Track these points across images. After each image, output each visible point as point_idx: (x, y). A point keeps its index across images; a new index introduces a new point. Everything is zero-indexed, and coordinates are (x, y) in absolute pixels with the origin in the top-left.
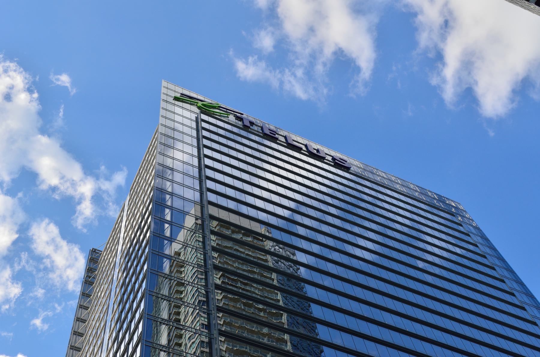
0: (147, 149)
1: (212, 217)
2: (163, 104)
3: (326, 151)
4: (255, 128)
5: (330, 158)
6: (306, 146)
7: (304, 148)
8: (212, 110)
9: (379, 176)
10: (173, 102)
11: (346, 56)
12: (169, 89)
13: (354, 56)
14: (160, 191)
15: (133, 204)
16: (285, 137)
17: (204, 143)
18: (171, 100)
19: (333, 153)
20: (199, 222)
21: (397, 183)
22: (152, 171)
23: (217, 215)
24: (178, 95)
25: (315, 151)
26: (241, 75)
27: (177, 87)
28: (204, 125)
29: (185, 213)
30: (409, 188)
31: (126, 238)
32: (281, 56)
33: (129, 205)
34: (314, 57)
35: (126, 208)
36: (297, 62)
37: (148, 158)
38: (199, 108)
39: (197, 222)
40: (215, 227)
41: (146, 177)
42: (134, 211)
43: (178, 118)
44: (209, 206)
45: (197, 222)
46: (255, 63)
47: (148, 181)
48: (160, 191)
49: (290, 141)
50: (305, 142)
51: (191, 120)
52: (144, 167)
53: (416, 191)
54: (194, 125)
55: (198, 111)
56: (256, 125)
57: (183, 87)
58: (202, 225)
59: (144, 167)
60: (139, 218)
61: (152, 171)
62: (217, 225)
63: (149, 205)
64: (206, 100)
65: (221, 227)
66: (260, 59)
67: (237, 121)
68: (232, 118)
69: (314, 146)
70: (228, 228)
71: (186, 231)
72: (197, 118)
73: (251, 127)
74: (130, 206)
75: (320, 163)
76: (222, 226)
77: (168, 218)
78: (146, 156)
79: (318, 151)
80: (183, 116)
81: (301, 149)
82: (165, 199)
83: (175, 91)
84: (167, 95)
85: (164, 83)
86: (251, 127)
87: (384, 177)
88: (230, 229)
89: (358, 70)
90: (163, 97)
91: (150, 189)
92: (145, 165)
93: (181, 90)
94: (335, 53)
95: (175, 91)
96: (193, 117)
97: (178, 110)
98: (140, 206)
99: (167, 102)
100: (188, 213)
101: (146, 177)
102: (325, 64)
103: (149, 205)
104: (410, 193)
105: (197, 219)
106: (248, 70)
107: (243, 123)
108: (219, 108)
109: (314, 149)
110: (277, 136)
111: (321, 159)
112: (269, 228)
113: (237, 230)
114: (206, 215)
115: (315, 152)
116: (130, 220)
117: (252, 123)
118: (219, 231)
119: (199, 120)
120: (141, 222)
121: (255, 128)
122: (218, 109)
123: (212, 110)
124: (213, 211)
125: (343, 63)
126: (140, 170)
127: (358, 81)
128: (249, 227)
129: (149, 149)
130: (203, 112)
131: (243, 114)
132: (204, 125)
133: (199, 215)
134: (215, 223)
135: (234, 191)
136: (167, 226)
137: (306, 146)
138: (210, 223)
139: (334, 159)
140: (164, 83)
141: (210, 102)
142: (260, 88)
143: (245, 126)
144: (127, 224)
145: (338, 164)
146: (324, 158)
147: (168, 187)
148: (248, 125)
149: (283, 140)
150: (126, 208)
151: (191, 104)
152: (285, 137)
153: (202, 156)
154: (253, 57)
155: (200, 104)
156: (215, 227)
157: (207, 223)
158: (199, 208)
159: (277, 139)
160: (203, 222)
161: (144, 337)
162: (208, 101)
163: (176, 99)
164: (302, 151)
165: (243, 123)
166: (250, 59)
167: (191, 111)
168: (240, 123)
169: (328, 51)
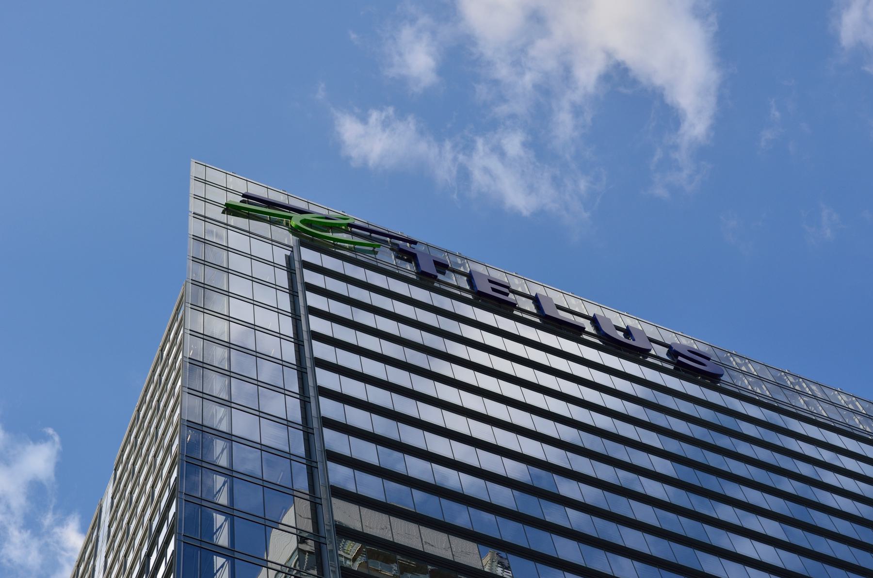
0: (158, 352)
1: (344, 533)
2: (196, 188)
3: (651, 331)
4: (453, 279)
5: (662, 352)
6: (594, 320)
7: (589, 328)
8: (330, 235)
9: (802, 393)
10: (224, 218)
11: (635, 82)
12: (21, 549)
13: (658, 81)
14: (199, 433)
15: (124, 503)
16: (536, 300)
17: (312, 328)
18: (216, 213)
19: (670, 338)
20: (310, 546)
21: (798, 392)
22: (173, 411)
23: (358, 527)
24: (236, 200)
25: (621, 334)
26: (354, 153)
27: (230, 178)
28: (312, 278)
29: (271, 524)
30: (833, 404)
31: (112, 567)
32: (459, 101)
33: (114, 508)
34: (546, 93)
35: (106, 518)
36: (503, 110)
37: (160, 375)
38: (294, 231)
39: (302, 546)
40: (354, 560)
41: (157, 428)
42: (128, 523)
43: (238, 263)
44: (334, 501)
45: (302, 546)
46: (386, 124)
47: (163, 439)
48: (199, 433)
49: (549, 311)
50: (592, 310)
51: (274, 265)
52: (151, 401)
53: (856, 412)
54: (283, 278)
55: (291, 239)
56: (454, 271)
57: (247, 175)
58: (318, 557)
59: (151, 401)
60: (141, 544)
61: (173, 411)
62: (359, 553)
63: (170, 472)
64: (312, 208)
65: (369, 557)
66: (401, 115)
67: (399, 261)
68: (387, 257)
69: (616, 319)
70: (388, 561)
71: (272, 573)
72: (289, 259)
73: (440, 277)
74: (116, 511)
75: (574, 344)
76: (371, 555)
77: (223, 539)
78: (154, 371)
79: (627, 332)
80: (252, 257)
81: (581, 329)
82: (211, 521)
83: (227, 189)
84: (205, 200)
85: (196, 170)
86: (440, 277)
87: (815, 397)
88: (394, 561)
89: (671, 117)
90: (196, 206)
91: (169, 462)
92: (152, 397)
93: (242, 186)
94: (605, 78)
95: (227, 189)
96: (280, 256)
97: (236, 240)
98: (146, 479)
99: (205, 218)
100: (276, 524)
101: (157, 428)
102: (577, 111)
103: (170, 472)
104: (835, 415)
105: (302, 540)
106: (371, 140)
107: (417, 265)
108: (350, 227)
109: (618, 328)
110: (511, 297)
111: (638, 355)
112: (503, 554)
113: (413, 564)
114: (326, 527)
115: (620, 335)
116: (118, 551)
117: (442, 267)
118: (365, 571)
119: (297, 265)
120: (149, 555)
121: (453, 279)
122: (346, 232)
123: (330, 235)
124: (346, 514)
125: (630, 101)
126: (139, 411)
127: (676, 147)
128: (448, 555)
129: (162, 350)
130: (303, 243)
131: (415, 243)
132: (312, 278)
133: (308, 526)
134: (352, 548)
135: (367, 414)
136: (219, 561)
137: (594, 320)
138: (337, 549)
139: (673, 353)
140: (196, 170)
141: (325, 212)
142: (409, 180)
143: (421, 274)
144: (113, 530)
145: (683, 364)
146: (646, 352)
147: (218, 417)
148: (432, 270)
149: (529, 306)
150: (106, 518)
151: (271, 222)
152: (536, 300)
153: (309, 364)
154: (381, 110)
155: (296, 220)
156: (354, 560)
157: (329, 547)
158: (305, 507)
159: (513, 305)
160: (319, 545)
161: (182, 487)
162: (319, 210)
163: (230, 209)
164: (585, 337)
165: (417, 265)
166: (375, 116)
167: (273, 242)
168: (408, 266)
169: (587, 75)
